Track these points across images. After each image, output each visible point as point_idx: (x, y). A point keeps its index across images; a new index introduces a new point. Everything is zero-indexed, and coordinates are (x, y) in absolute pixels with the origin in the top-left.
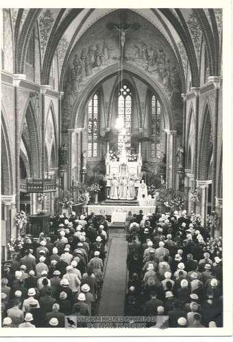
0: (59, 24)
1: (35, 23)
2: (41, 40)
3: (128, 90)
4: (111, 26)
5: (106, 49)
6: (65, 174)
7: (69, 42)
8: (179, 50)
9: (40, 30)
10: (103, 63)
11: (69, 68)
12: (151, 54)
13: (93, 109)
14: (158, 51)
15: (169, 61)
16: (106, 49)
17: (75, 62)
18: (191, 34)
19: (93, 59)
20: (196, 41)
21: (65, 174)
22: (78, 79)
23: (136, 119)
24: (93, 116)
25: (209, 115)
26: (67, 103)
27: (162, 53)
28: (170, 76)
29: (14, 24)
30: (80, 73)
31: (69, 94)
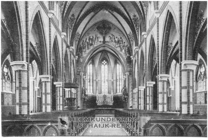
1: (68, 19)
7: (80, 34)
8: (129, 37)
10: (95, 44)
14: (120, 38)
19: (91, 42)
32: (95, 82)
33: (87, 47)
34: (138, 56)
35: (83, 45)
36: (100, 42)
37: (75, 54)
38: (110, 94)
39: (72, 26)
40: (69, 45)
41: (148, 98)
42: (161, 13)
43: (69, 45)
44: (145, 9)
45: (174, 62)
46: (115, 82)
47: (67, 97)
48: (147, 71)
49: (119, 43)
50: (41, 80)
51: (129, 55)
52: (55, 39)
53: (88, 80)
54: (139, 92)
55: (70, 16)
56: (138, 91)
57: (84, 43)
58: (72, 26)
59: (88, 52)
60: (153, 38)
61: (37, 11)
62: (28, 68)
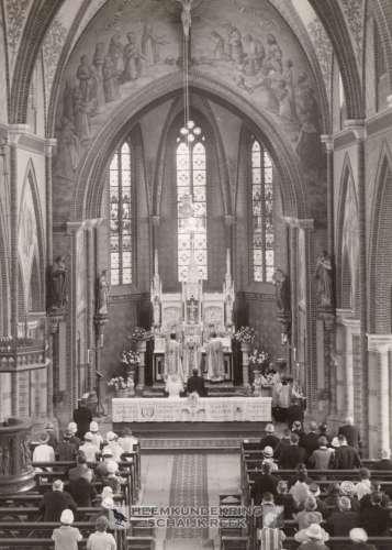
12: (249, 49)
16: (149, 42)
19: (120, 65)
22: (88, 110)
27: (274, 46)
28: (294, 97)
30: (93, 95)
31: (68, 144)
32: (143, 230)
33: (100, 88)
35: (82, 80)
36: (169, 62)
38: (220, 289)
46: (241, 227)
54: (371, 360)
57: (86, 69)
58: (18, 24)
59: (109, 112)
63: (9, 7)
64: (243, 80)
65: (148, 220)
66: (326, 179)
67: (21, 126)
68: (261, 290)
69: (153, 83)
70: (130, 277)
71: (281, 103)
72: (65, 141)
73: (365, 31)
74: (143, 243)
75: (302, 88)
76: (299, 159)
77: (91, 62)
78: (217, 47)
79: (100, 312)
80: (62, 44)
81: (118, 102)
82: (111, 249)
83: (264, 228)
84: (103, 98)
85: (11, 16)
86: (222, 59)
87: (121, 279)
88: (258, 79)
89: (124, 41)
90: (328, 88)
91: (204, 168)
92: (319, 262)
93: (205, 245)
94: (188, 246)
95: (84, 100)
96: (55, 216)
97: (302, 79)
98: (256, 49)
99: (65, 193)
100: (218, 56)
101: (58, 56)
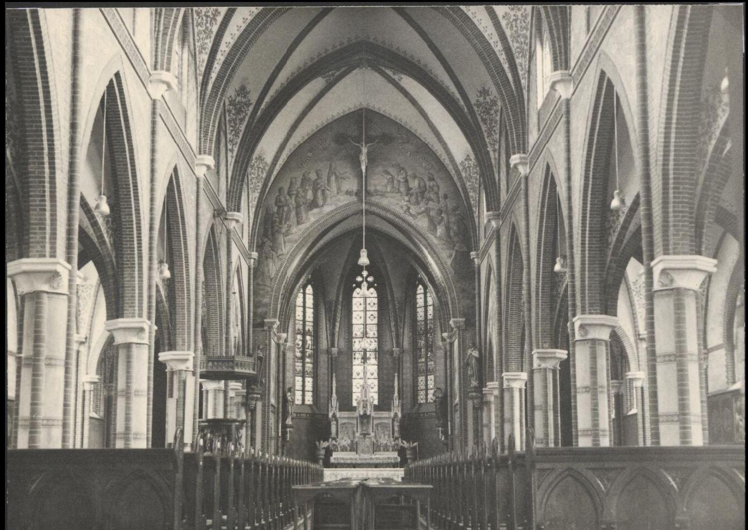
0: (259, 113)
2: (229, 136)
3: (371, 279)
4: (341, 139)
5: (333, 178)
6: (259, 405)
8: (464, 174)
9: (228, 118)
10: (329, 200)
11: (267, 213)
12: (414, 184)
13: (304, 312)
14: (426, 179)
15: (446, 197)
16: (333, 178)
17: (278, 201)
18: (481, 124)
19: (310, 195)
20: (490, 135)
21: (259, 405)
22: (284, 230)
23: (388, 339)
24: (304, 325)
25: (517, 239)
26: (263, 273)
27: (432, 183)
28: (449, 222)
29: (200, 78)
30: (287, 219)
31: (267, 258)
32: (323, 358)
33: (293, 213)
34: (498, 249)
35: (279, 207)
36: (348, 193)
37: (246, 241)
39: (236, 135)
40: (225, 206)
41: (538, 416)
42: (576, 80)
43: (225, 206)
44: (521, 65)
45: (633, 264)
47: (210, 416)
48: (536, 313)
49: (423, 197)
50: (111, 340)
51: (465, 249)
52: (171, 182)
53: (294, 352)
55: (231, 92)
56: (502, 391)
58: (236, 135)
60: (553, 178)
61: (112, 76)
62: (70, 287)
63: (230, 121)
64: (409, 208)
65: (328, 352)
66: (474, 289)
67: (236, 213)
68: (423, 410)
69: (336, 209)
70: (311, 399)
71: (438, 227)
72: (264, 255)
73: (500, 144)
74: (323, 370)
75: (455, 215)
76: (453, 272)
77: (286, 193)
78: (388, 182)
79: (287, 422)
80: (264, 175)
81: (307, 225)
82: (295, 373)
83: (427, 358)
84: (296, 222)
85: (231, 128)
86: (390, 192)
87: (303, 400)
88: (420, 208)
89: (313, 176)
90: (476, 215)
91: (376, 309)
92: (469, 352)
93: (376, 375)
94: (362, 375)
95: (280, 223)
96: (255, 313)
97: (455, 209)
98: (419, 184)
99: (263, 296)
100: (389, 189)
101: (260, 185)
